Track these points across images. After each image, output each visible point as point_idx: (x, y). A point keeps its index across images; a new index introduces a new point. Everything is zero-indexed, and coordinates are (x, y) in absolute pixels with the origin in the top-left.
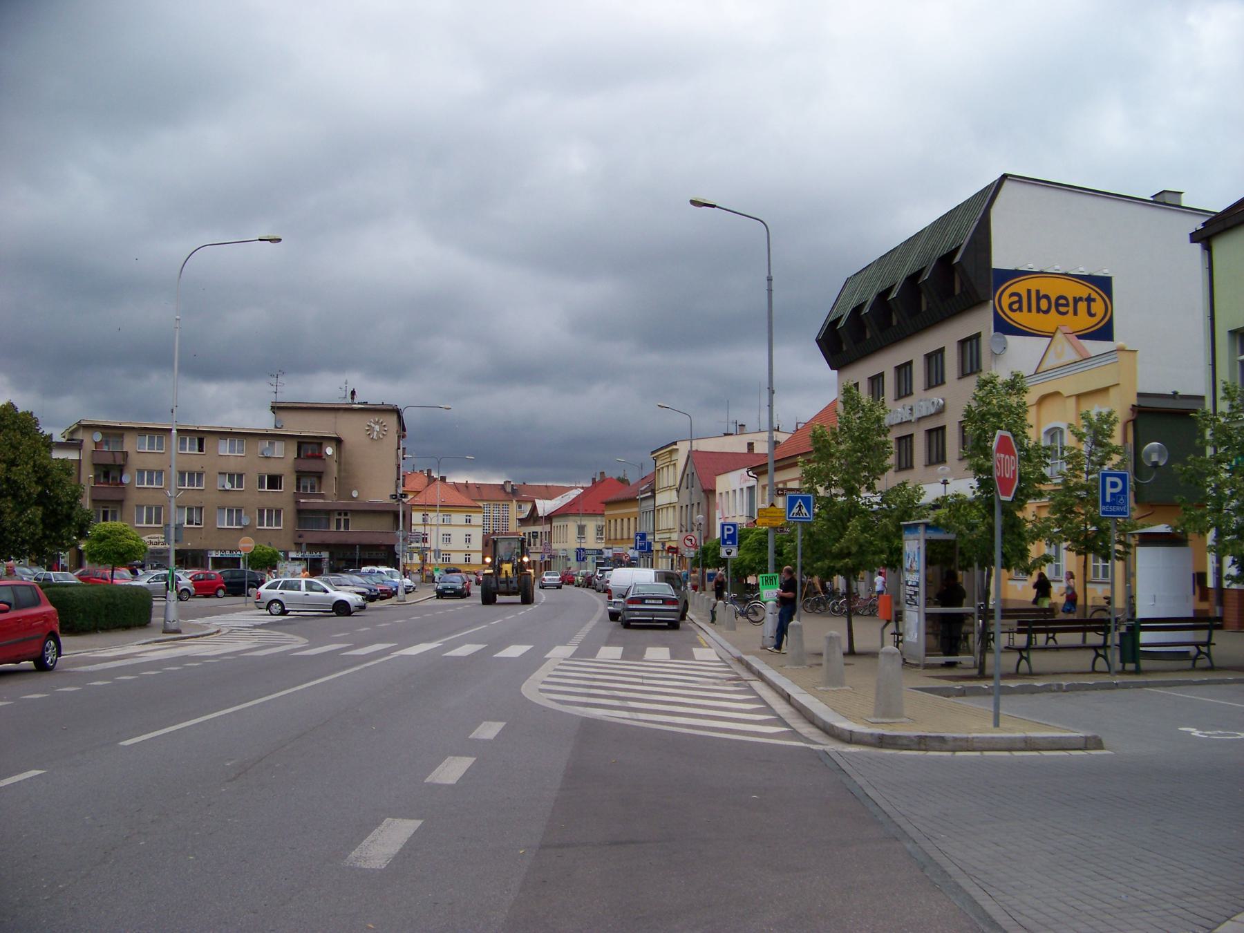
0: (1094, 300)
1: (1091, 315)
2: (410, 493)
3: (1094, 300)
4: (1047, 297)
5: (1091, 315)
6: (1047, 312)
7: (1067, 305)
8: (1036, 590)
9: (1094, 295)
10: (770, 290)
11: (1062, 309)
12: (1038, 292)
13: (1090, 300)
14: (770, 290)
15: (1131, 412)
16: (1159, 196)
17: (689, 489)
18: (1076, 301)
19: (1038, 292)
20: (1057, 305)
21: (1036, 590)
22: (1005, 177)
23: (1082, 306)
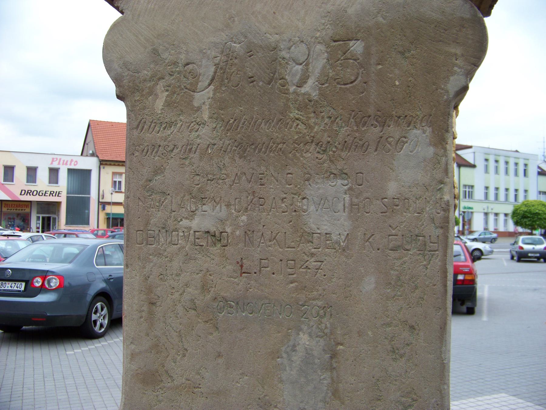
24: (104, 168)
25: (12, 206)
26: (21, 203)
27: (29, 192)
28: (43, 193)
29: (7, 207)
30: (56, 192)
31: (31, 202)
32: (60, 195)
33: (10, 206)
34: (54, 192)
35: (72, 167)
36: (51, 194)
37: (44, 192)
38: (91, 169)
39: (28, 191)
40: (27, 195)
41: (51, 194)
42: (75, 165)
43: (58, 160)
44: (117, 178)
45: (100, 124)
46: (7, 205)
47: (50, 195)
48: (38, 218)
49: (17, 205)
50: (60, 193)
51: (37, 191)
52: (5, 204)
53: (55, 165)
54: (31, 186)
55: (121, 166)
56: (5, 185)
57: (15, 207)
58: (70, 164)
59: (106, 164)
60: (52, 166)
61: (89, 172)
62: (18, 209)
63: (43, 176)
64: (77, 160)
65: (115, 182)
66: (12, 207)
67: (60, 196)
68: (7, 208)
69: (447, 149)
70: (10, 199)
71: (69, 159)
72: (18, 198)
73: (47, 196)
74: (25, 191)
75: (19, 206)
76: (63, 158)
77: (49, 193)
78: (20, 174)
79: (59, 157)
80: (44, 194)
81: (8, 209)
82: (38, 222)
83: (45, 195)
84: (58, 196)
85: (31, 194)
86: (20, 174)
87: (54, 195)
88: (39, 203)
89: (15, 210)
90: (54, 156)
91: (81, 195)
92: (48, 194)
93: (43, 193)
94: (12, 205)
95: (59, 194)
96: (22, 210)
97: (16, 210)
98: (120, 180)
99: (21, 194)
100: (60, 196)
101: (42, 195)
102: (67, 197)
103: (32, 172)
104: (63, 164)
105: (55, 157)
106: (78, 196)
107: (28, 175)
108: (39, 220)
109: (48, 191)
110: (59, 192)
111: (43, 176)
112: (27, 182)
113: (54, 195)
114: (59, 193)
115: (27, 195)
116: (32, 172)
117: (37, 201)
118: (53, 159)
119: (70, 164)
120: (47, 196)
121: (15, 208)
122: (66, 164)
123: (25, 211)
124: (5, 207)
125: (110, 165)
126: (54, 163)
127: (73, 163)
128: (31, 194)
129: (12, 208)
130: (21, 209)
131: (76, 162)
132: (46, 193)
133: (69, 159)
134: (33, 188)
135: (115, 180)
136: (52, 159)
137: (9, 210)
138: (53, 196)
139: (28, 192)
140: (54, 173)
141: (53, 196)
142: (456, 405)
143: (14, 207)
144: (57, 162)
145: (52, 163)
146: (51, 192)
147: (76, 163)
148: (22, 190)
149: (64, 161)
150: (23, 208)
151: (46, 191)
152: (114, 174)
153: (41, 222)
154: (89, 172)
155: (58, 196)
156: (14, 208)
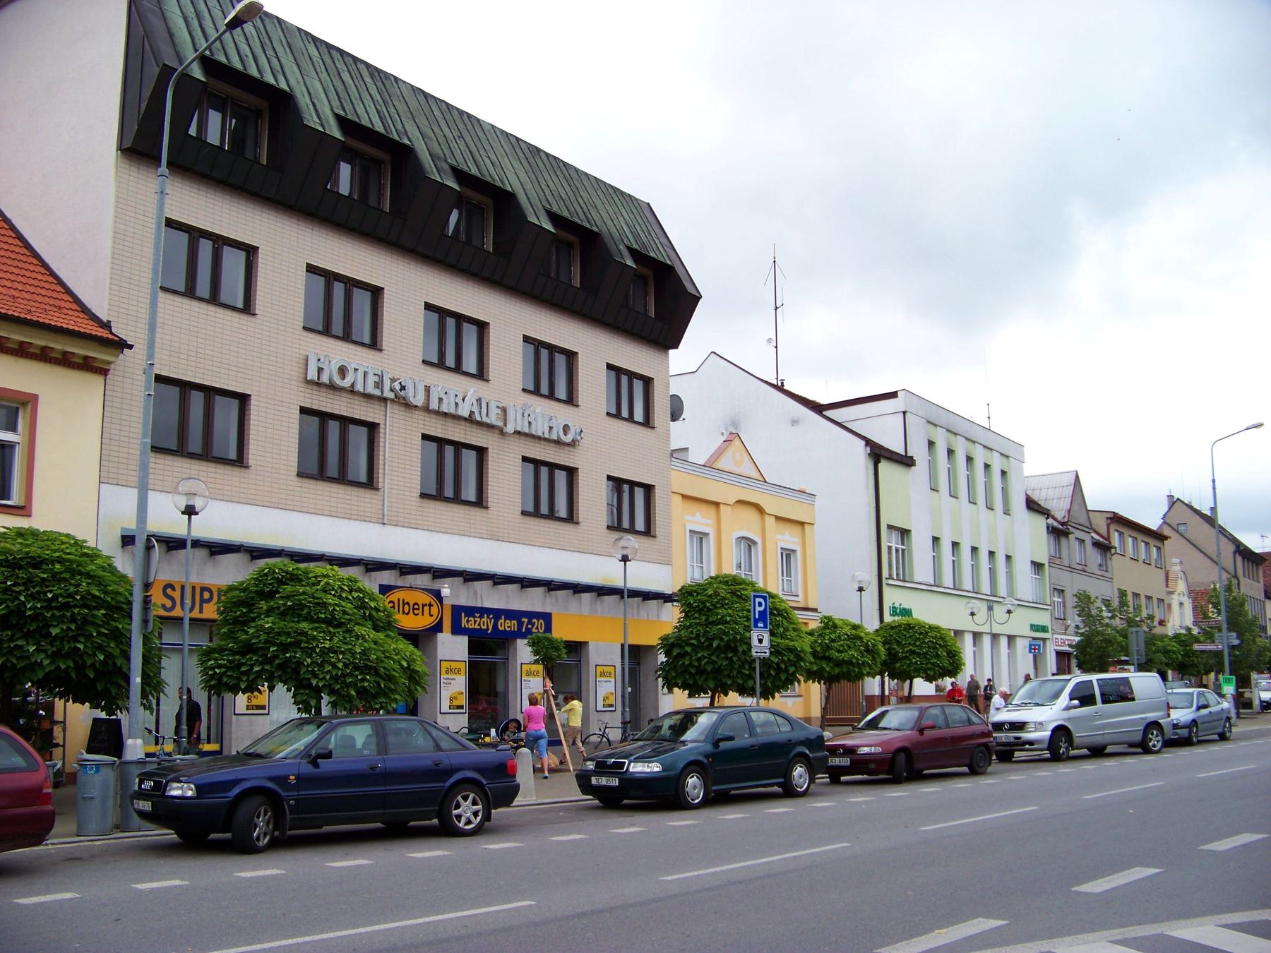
0: (432, 605)
1: (431, 616)
2: (154, 718)
3: (432, 605)
4: (408, 603)
5: (431, 616)
6: (408, 614)
7: (418, 609)
8: (731, 693)
9: (433, 602)
10: (1214, 488)
11: (416, 612)
12: (403, 600)
13: (430, 605)
14: (1214, 488)
15: (1052, 538)
16: (1080, 497)
17: (1101, 524)
18: (424, 606)
19: (403, 600)
20: (414, 609)
21: (731, 693)
22: (950, 496)
23: (426, 609)
30: (399, 600)
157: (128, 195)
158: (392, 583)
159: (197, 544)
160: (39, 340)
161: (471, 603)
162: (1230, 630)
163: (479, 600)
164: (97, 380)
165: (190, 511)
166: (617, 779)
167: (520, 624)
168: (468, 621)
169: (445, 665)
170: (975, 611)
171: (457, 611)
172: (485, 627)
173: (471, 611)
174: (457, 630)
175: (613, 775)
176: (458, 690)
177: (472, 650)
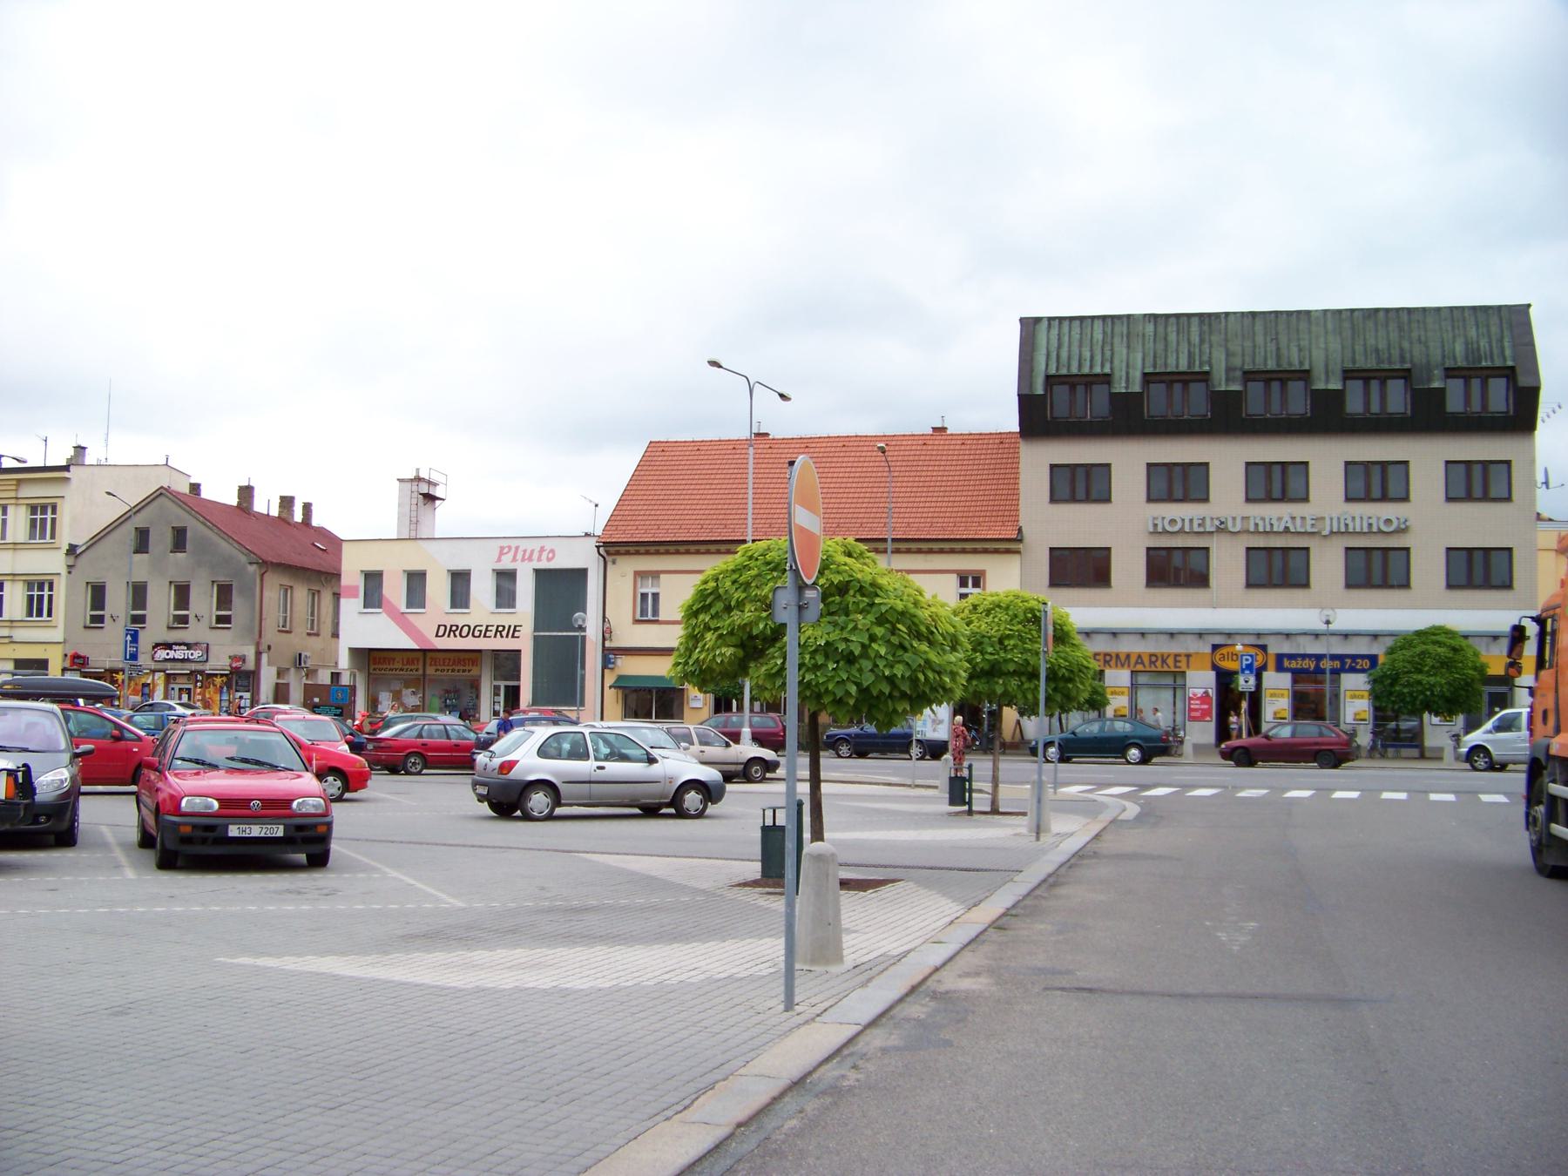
24: (614, 562)
25: (384, 661)
26: (385, 654)
27: (453, 630)
28: (481, 631)
29: (436, 665)
30: (510, 627)
31: (480, 651)
32: (516, 634)
33: (442, 663)
34: (504, 627)
35: (544, 565)
36: (499, 631)
37: (483, 629)
38: (585, 567)
39: (451, 626)
40: (449, 636)
41: (499, 631)
42: (549, 560)
43: (513, 550)
44: (647, 587)
45: (931, 442)
46: (434, 662)
47: (495, 636)
48: (496, 693)
49: (454, 661)
50: (490, 628)
51: (469, 626)
52: (431, 658)
53: (507, 564)
54: (455, 615)
55: (662, 554)
56: (408, 616)
57: (451, 663)
58: (539, 559)
59: (618, 553)
60: (500, 566)
61: (582, 574)
62: (457, 668)
63: (482, 589)
64: (553, 547)
65: (644, 596)
66: (444, 665)
67: (518, 637)
68: (435, 667)
69: (247, 484)
70: (418, 648)
71: (536, 545)
72: (431, 643)
73: (490, 637)
74: (445, 626)
75: (459, 662)
76: (524, 544)
77: (494, 629)
78: (438, 590)
79: (514, 543)
80: (483, 632)
81: (437, 670)
82: (497, 698)
83: (485, 636)
84: (513, 636)
85: (457, 633)
86: (438, 590)
87: (504, 633)
88: (496, 652)
89: (450, 673)
90: (506, 544)
91: (566, 631)
92: (492, 634)
93: (481, 631)
94: (444, 659)
95: (514, 632)
96: (464, 671)
97: (453, 671)
98: (654, 590)
99: (437, 636)
100: (518, 637)
101: (479, 636)
102: (535, 638)
103: (460, 580)
104: (523, 560)
105: (505, 543)
106: (560, 634)
107: (1487, 584)
108: (499, 695)
109: (493, 626)
110: (515, 627)
111: (482, 589)
112: (498, 606)
113: (504, 633)
114: (515, 631)
115: (449, 636)
116: (460, 580)
117: (493, 651)
118: (502, 548)
119: (539, 559)
120: (490, 637)
121: (451, 668)
122: (530, 559)
123: (471, 673)
124: (431, 665)
125: (628, 553)
126: (503, 557)
127: (544, 556)
128: (457, 633)
129: (445, 668)
130: (462, 668)
131: (552, 551)
132: (487, 630)
133: (536, 545)
134: (460, 621)
135: (644, 590)
136: (499, 549)
137: (438, 673)
138: (502, 636)
139: (450, 630)
140: (505, 579)
141: (502, 636)
142: (277, 1140)
143: (448, 665)
144: (511, 555)
145: (499, 560)
146: (498, 626)
147: (551, 555)
148: (439, 626)
149: (525, 551)
150: (467, 668)
151: (487, 626)
152: (637, 574)
153: (502, 698)
154: (582, 574)
155: (513, 636)
156: (448, 668)
157: (890, 471)
158: (1223, 643)
159: (1333, 634)
160: (978, 546)
161: (1293, 651)
162: (801, 747)
163: (1301, 647)
164: (1016, 557)
165: (1328, 622)
166: (281, 827)
167: (1343, 664)
168: (1290, 664)
169: (1348, 693)
170: (1331, 620)
171: (1280, 658)
172: (1307, 666)
173: (1292, 657)
174: (1280, 668)
175: (275, 819)
176: (1122, 705)
177: (1295, 681)
